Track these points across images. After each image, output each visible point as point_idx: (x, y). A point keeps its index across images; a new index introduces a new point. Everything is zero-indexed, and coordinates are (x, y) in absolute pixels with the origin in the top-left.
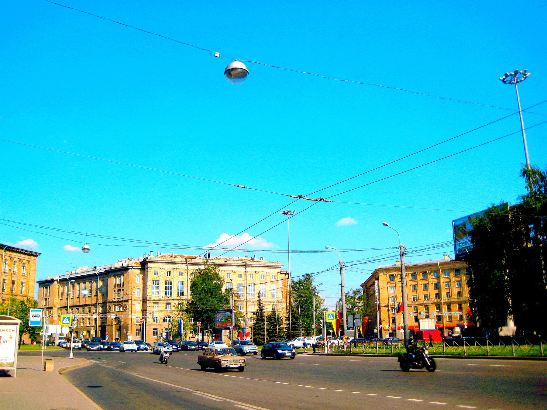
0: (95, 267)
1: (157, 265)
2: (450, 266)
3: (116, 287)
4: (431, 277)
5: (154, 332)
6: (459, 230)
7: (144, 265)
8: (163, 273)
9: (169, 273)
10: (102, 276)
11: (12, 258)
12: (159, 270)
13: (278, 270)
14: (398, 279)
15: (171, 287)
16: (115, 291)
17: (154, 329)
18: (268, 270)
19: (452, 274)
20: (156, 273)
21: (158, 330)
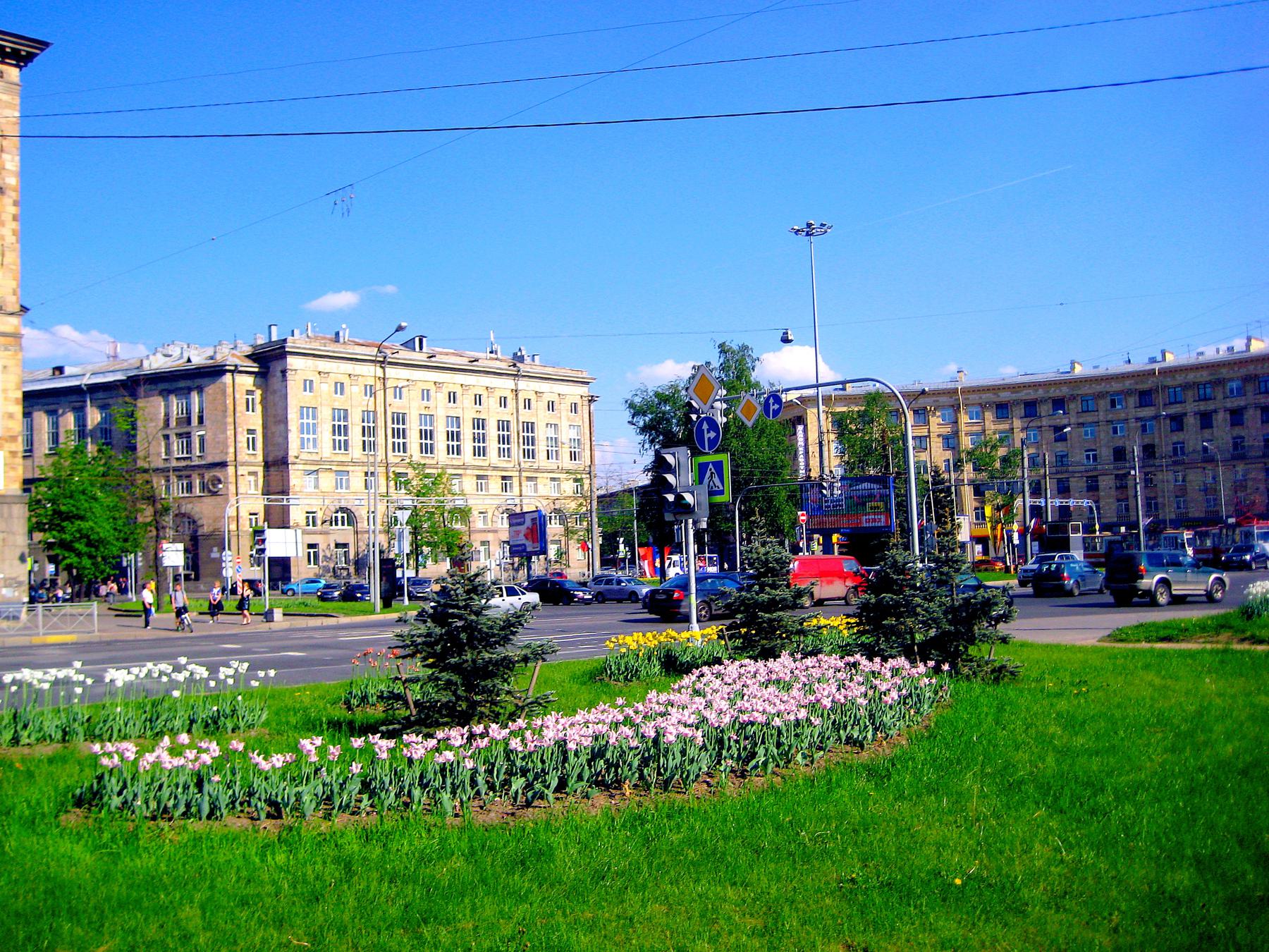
0: (60, 370)
1: (310, 362)
2: (984, 396)
3: (173, 423)
4: (935, 421)
6: (744, 348)
7: (269, 361)
10: (100, 395)
12: (316, 379)
16: (167, 437)
17: (311, 546)
19: (989, 416)
21: (322, 546)
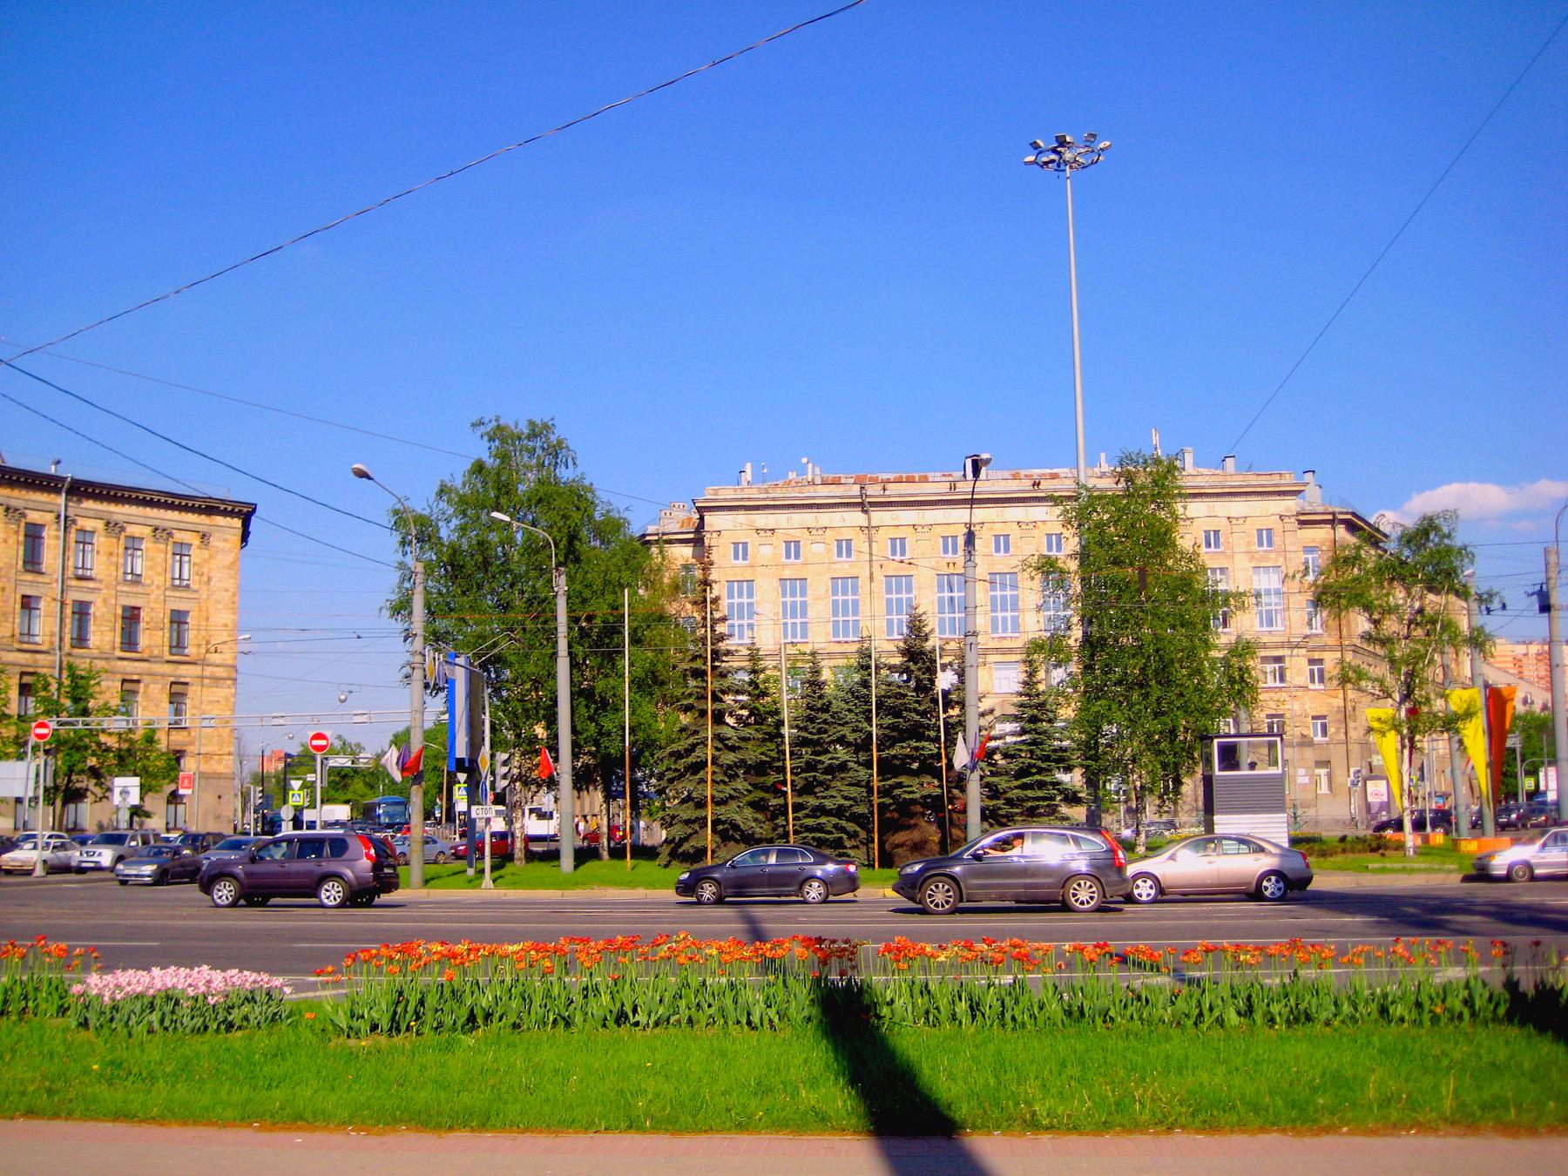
1: (742, 517)
5: (1312, 672)
8: (766, 552)
9: (793, 548)
11: (113, 527)
12: (753, 540)
13: (1290, 505)
14: (20, 825)
15: (804, 605)
18: (1237, 507)
20: (741, 550)
